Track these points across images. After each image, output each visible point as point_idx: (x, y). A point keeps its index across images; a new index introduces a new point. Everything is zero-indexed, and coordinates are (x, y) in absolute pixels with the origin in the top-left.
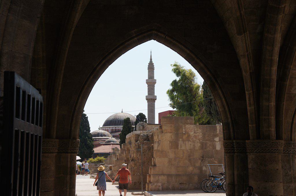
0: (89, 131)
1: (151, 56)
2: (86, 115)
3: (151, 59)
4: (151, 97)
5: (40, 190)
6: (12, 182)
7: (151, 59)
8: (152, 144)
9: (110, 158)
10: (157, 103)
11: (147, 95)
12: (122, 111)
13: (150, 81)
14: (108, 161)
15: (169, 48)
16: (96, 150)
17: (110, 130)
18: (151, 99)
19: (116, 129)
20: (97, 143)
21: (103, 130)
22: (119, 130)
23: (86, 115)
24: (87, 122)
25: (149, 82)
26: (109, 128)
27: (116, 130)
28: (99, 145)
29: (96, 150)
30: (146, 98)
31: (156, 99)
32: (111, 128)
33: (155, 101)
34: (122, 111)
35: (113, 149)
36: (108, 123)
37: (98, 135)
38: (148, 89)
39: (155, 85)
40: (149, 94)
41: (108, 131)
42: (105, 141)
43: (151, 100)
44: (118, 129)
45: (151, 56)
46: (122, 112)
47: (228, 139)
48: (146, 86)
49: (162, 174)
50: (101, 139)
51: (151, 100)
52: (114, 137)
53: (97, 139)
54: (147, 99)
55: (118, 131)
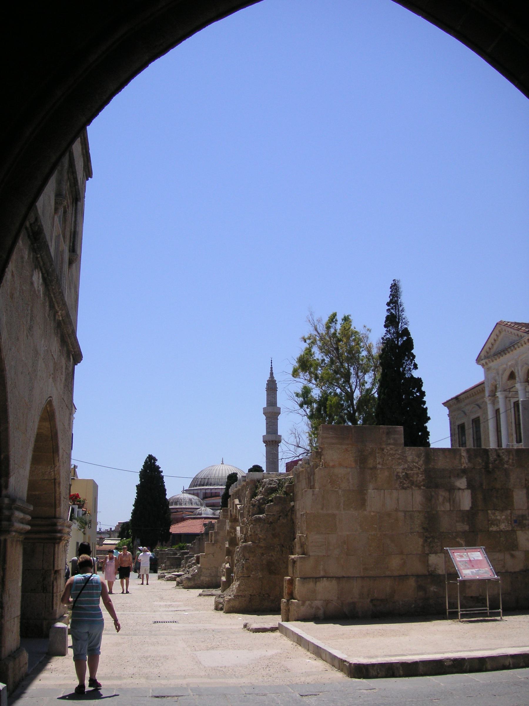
1: (271, 368)
3: (272, 374)
4: (272, 438)
6: (487, 618)
7: (272, 374)
8: (292, 504)
10: (282, 448)
11: (265, 434)
13: (271, 409)
15: (420, 18)
16: (175, 529)
18: (272, 441)
19: (211, 493)
20: (180, 516)
21: (190, 494)
26: (199, 491)
28: (183, 519)
29: (175, 529)
31: (280, 442)
34: (222, 462)
35: (205, 525)
36: (198, 482)
37: (177, 501)
38: (267, 424)
39: (279, 417)
40: (268, 432)
41: (197, 495)
42: (192, 512)
43: (272, 442)
45: (271, 368)
48: (262, 421)
49: (323, 577)
50: (186, 510)
51: (272, 442)
52: (208, 505)
53: (179, 510)
54: (264, 442)
55: (216, 495)
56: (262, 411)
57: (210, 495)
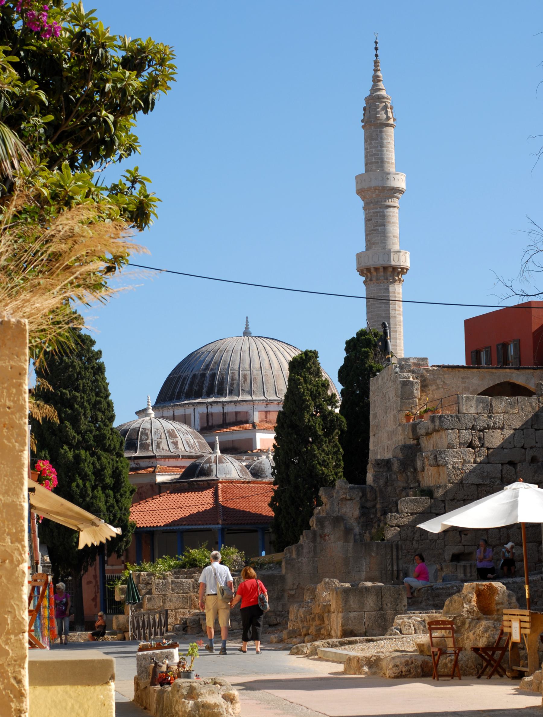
0: (112, 418)
2: (93, 343)
5: (522, 553)
9: (314, 540)
12: (247, 328)
14: (305, 560)
17: (197, 416)
18: (385, 268)
19: (224, 415)
22: (239, 419)
23: (93, 343)
24: (339, 377)
25: (369, 189)
26: (189, 411)
27: (224, 419)
30: (359, 263)
32: (202, 410)
33: (363, 278)
34: (247, 328)
41: (185, 420)
44: (237, 413)
46: (247, 333)
47: (466, 582)
48: (356, 210)
56: (353, 186)
57: (221, 422)
